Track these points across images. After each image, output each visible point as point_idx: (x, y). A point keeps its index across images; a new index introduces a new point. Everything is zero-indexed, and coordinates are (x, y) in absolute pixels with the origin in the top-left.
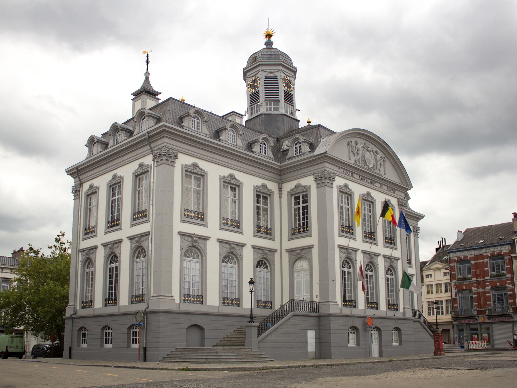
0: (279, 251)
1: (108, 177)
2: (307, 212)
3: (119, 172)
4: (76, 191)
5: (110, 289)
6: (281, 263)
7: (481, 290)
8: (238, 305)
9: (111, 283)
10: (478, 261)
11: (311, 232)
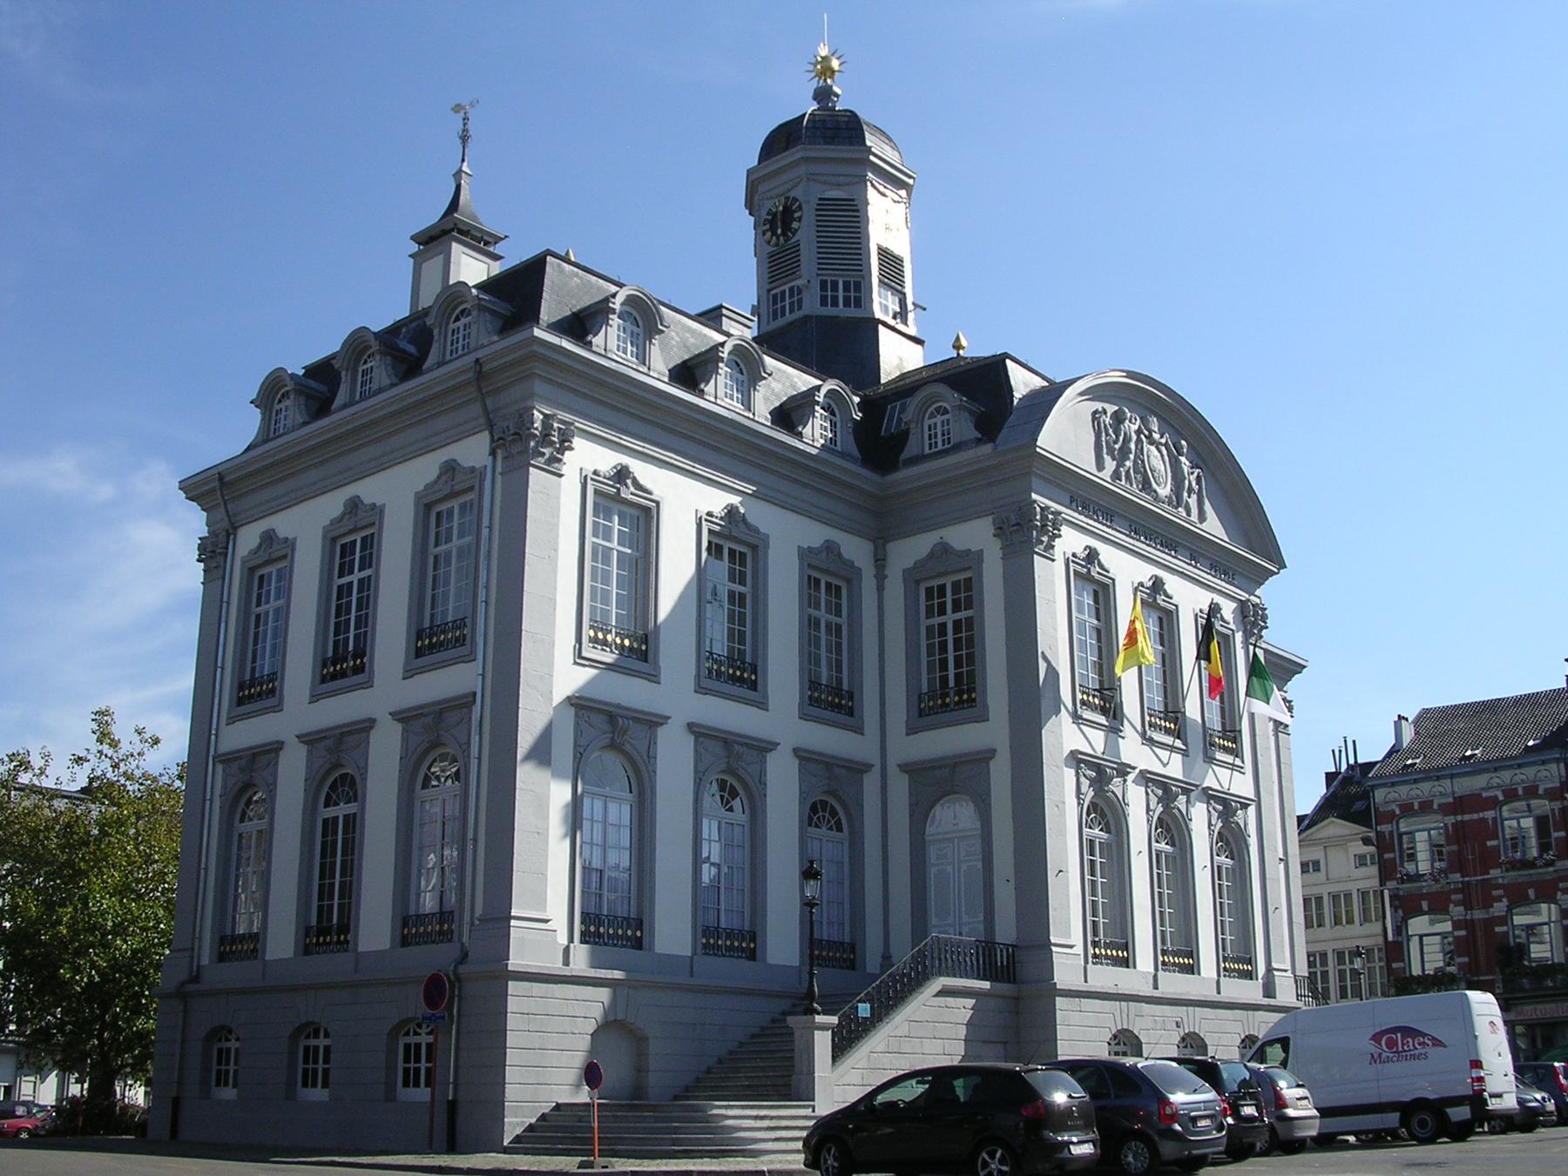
0: (877, 769)
1: (330, 506)
2: (970, 640)
3: (369, 490)
4: (213, 552)
5: (325, 892)
6: (885, 807)
7: (1478, 914)
8: (752, 955)
9: (326, 871)
10: (1467, 817)
11: (986, 706)
